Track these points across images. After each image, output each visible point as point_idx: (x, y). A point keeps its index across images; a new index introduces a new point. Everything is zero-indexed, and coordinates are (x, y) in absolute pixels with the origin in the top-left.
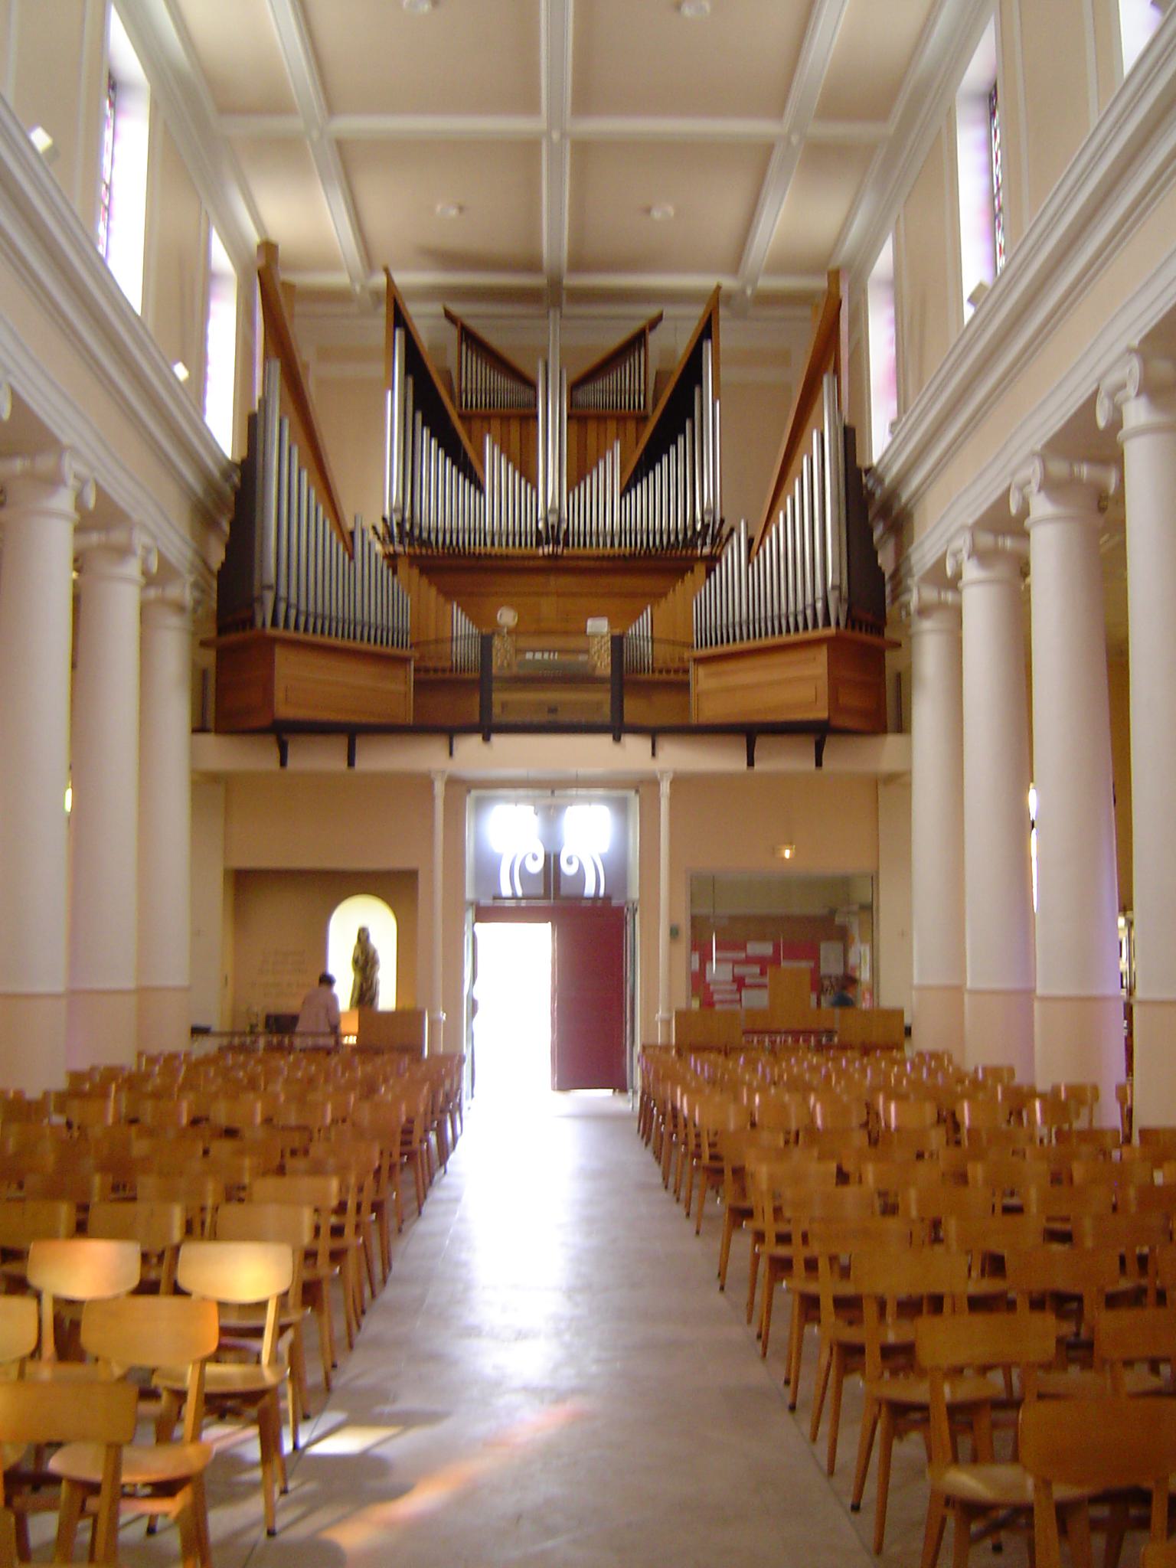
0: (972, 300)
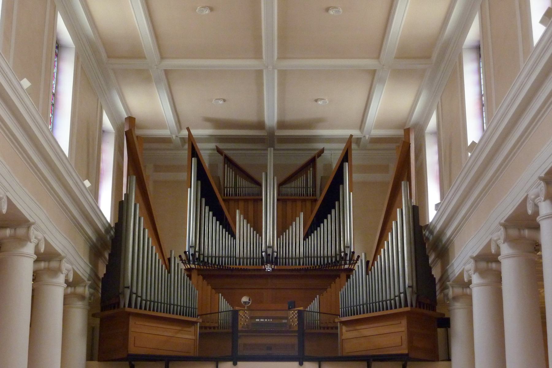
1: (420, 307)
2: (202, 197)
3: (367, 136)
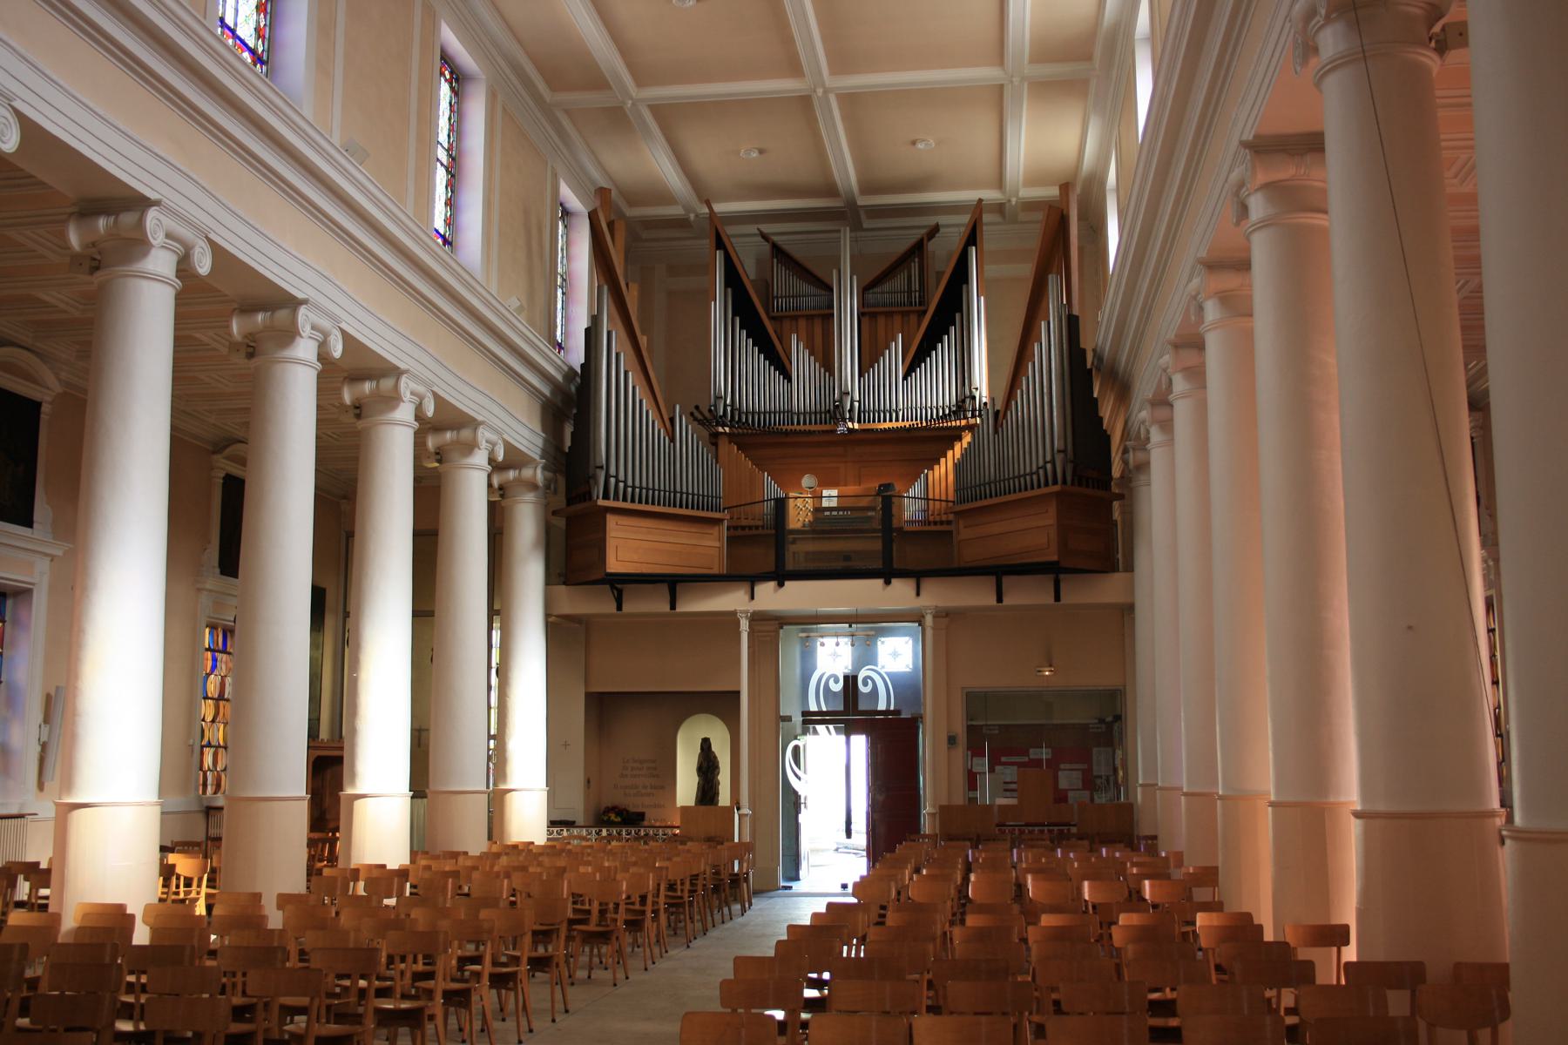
1: (1080, 485)
2: (734, 315)
3: (1014, 200)
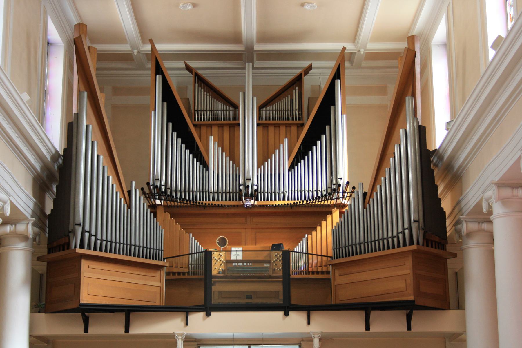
0: (494, 46)
1: (428, 246)
2: (168, 121)
3: (362, 51)
